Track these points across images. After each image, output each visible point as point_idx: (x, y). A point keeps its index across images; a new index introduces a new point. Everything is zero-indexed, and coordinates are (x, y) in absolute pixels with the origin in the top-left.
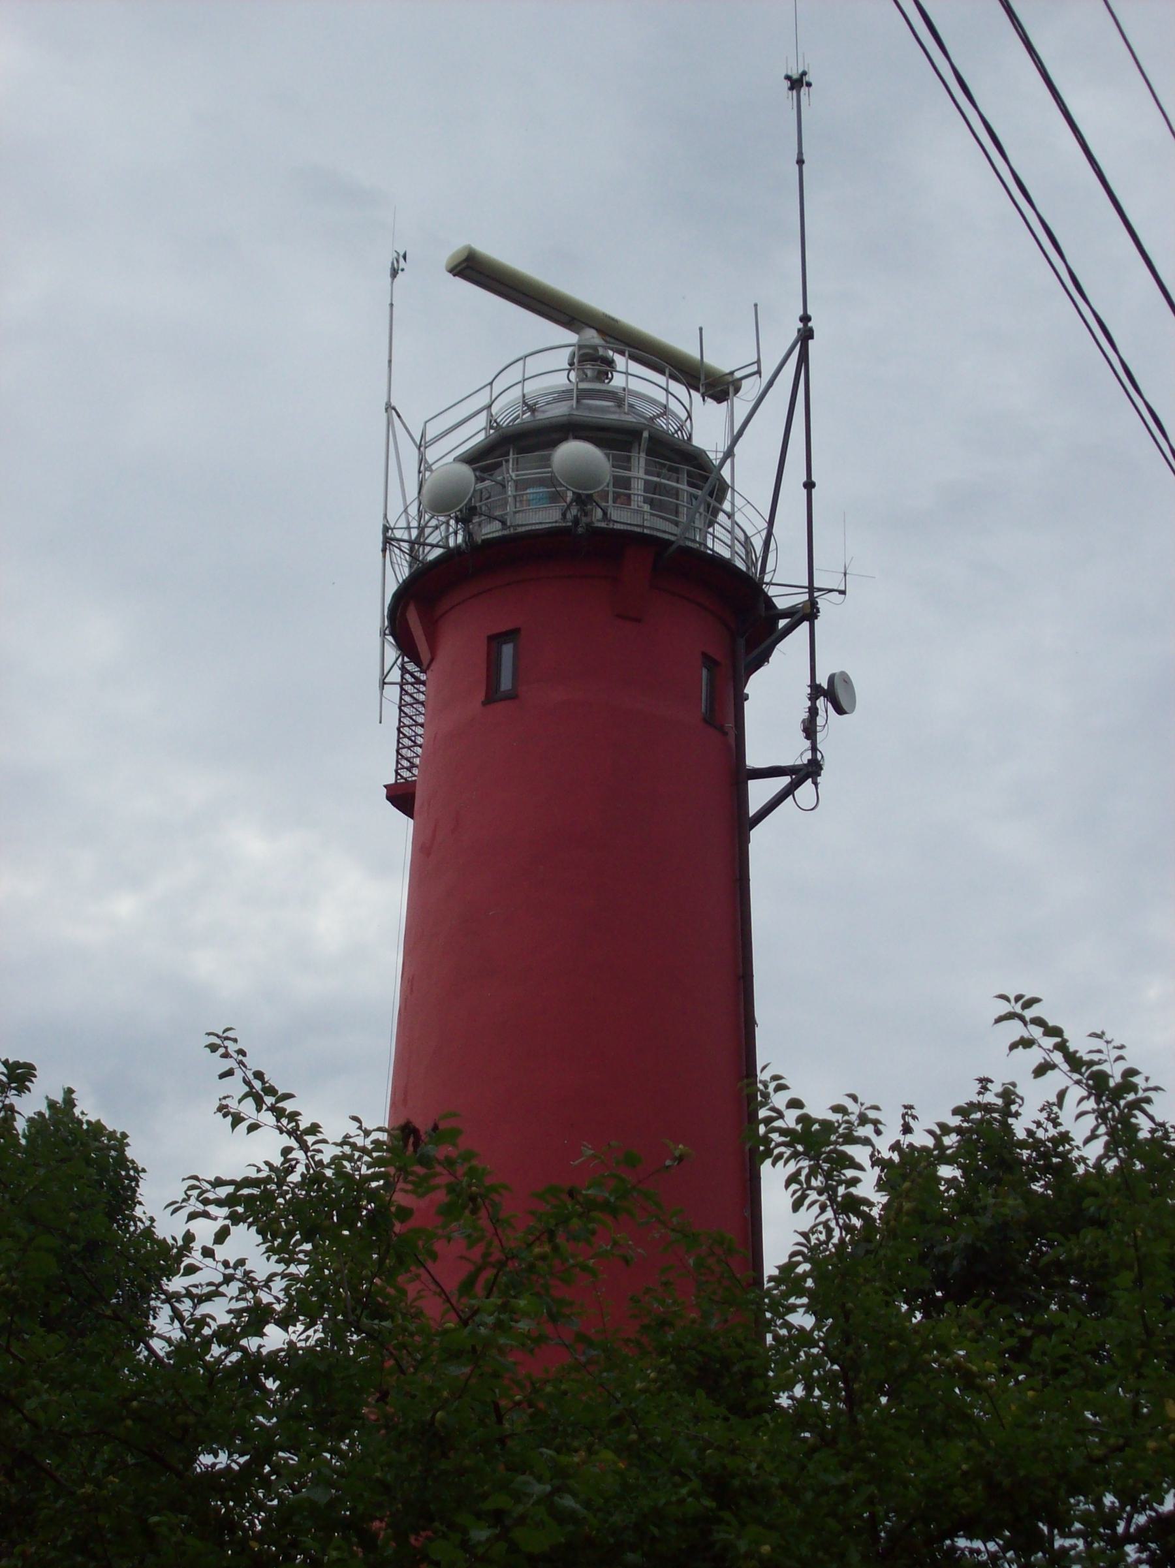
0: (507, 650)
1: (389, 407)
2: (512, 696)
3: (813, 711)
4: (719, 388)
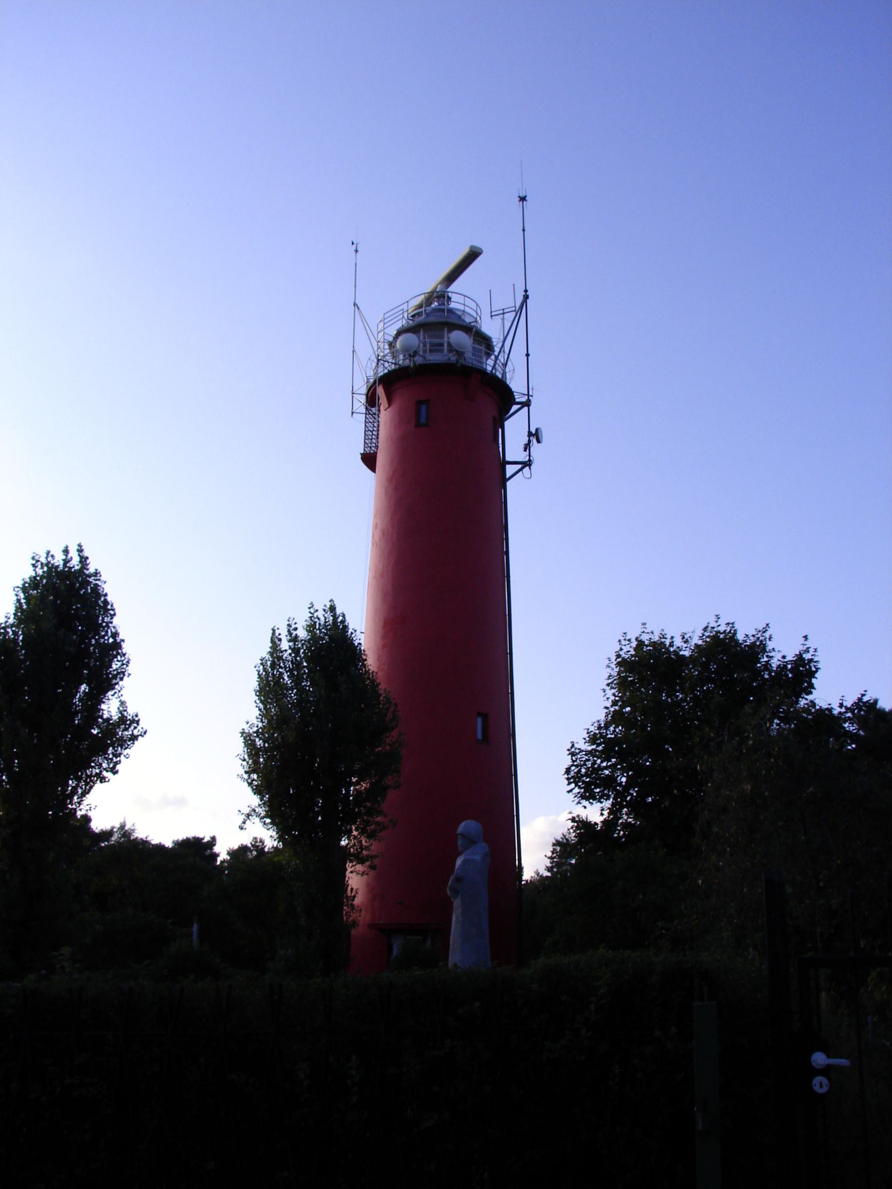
0: (424, 408)
1: (355, 304)
3: (529, 441)
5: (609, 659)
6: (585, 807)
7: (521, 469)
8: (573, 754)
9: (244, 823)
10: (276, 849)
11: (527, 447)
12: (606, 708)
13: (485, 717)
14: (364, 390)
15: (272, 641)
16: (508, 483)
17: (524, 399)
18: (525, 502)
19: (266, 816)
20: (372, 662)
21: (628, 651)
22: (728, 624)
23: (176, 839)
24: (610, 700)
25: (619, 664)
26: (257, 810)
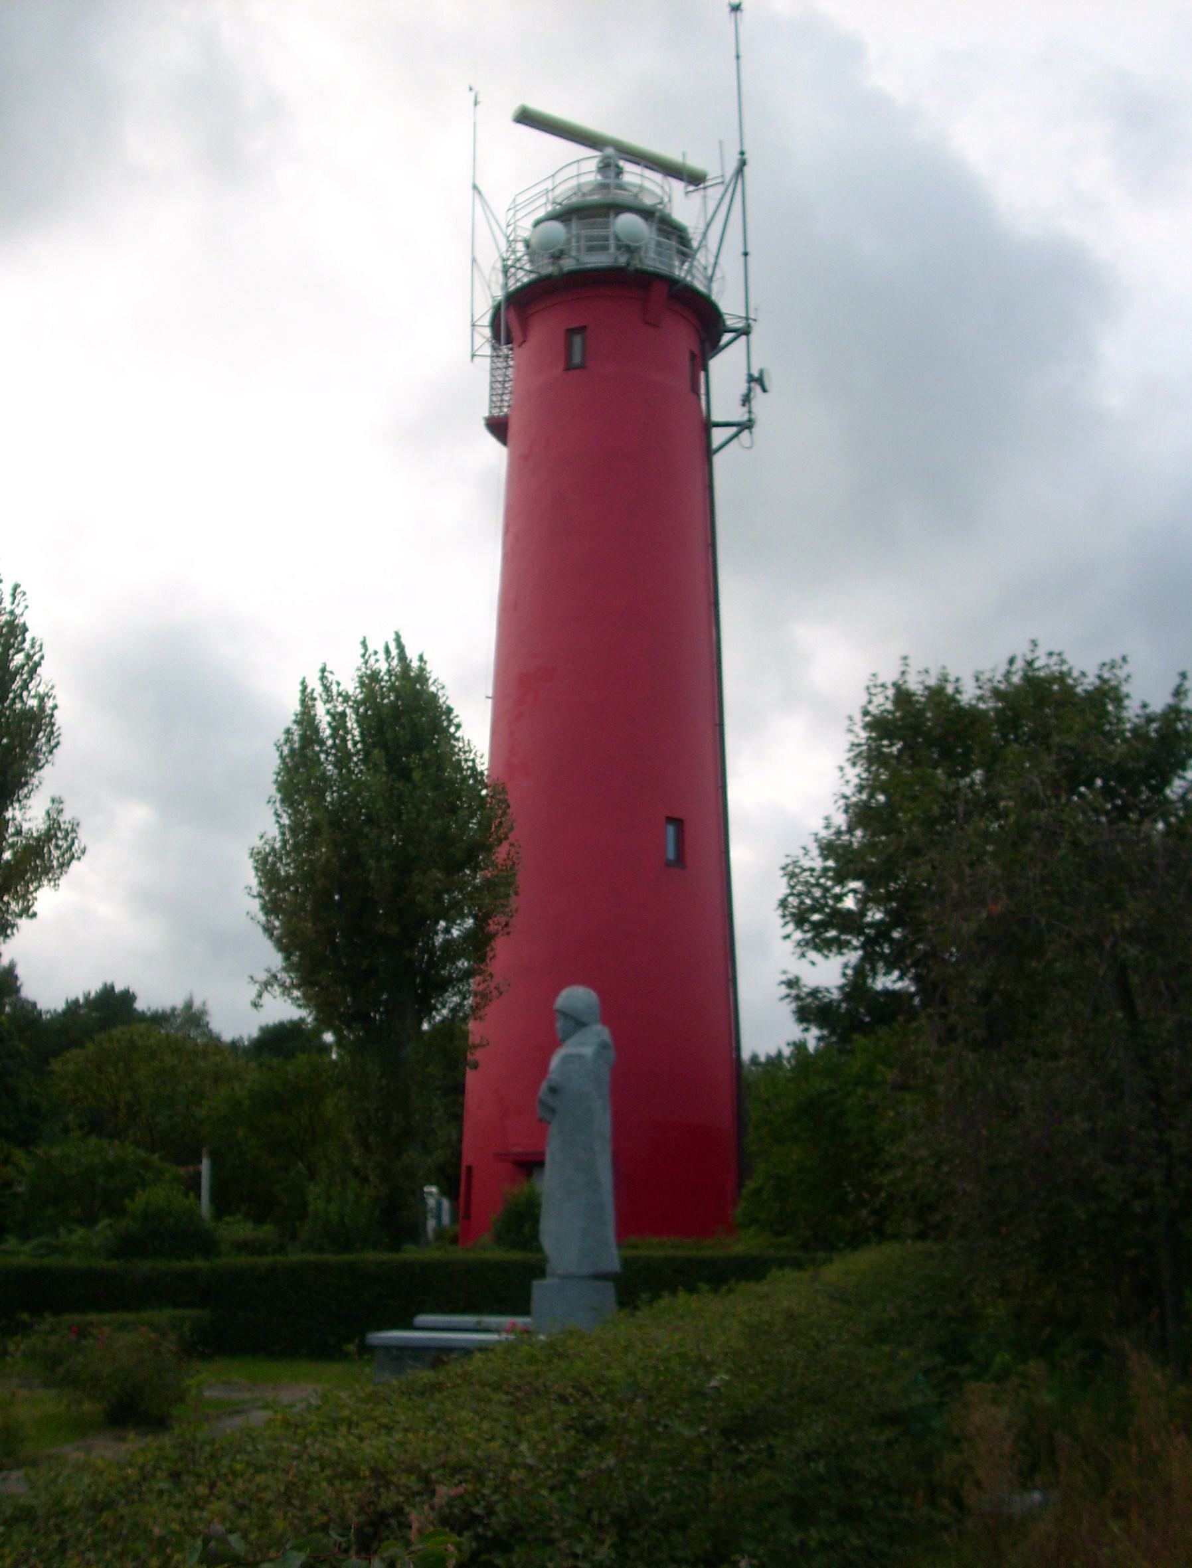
0: (577, 340)
1: (475, 187)
2: (583, 367)
3: (750, 390)
4: (695, 179)
5: (850, 718)
6: (813, 963)
7: (736, 435)
8: (792, 875)
9: (260, 996)
10: (278, 1041)
11: (746, 400)
12: (845, 797)
13: (678, 823)
14: (486, 320)
15: (303, 702)
16: (717, 459)
17: (741, 325)
18: (745, 485)
19: (294, 986)
20: (475, 732)
21: (883, 703)
22: (1050, 654)
23: (263, 1024)
24: (852, 784)
25: (868, 726)
26: (279, 976)
